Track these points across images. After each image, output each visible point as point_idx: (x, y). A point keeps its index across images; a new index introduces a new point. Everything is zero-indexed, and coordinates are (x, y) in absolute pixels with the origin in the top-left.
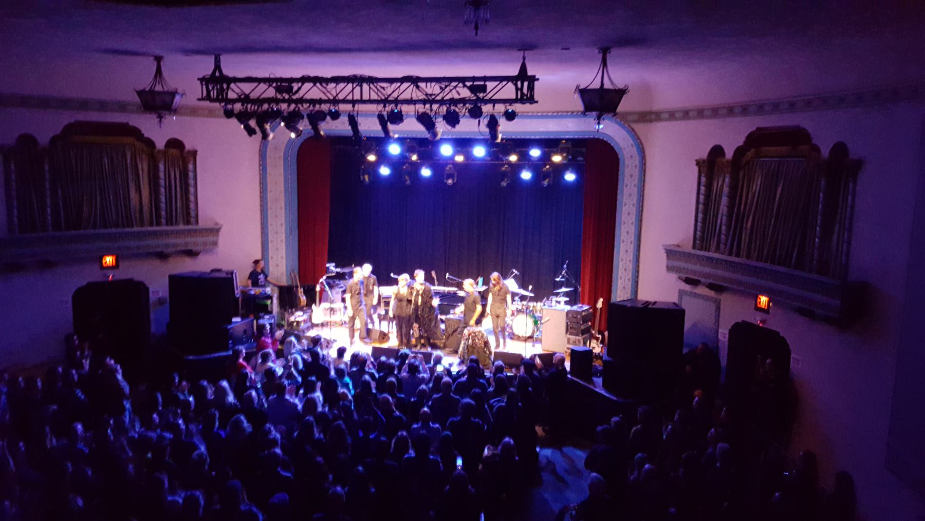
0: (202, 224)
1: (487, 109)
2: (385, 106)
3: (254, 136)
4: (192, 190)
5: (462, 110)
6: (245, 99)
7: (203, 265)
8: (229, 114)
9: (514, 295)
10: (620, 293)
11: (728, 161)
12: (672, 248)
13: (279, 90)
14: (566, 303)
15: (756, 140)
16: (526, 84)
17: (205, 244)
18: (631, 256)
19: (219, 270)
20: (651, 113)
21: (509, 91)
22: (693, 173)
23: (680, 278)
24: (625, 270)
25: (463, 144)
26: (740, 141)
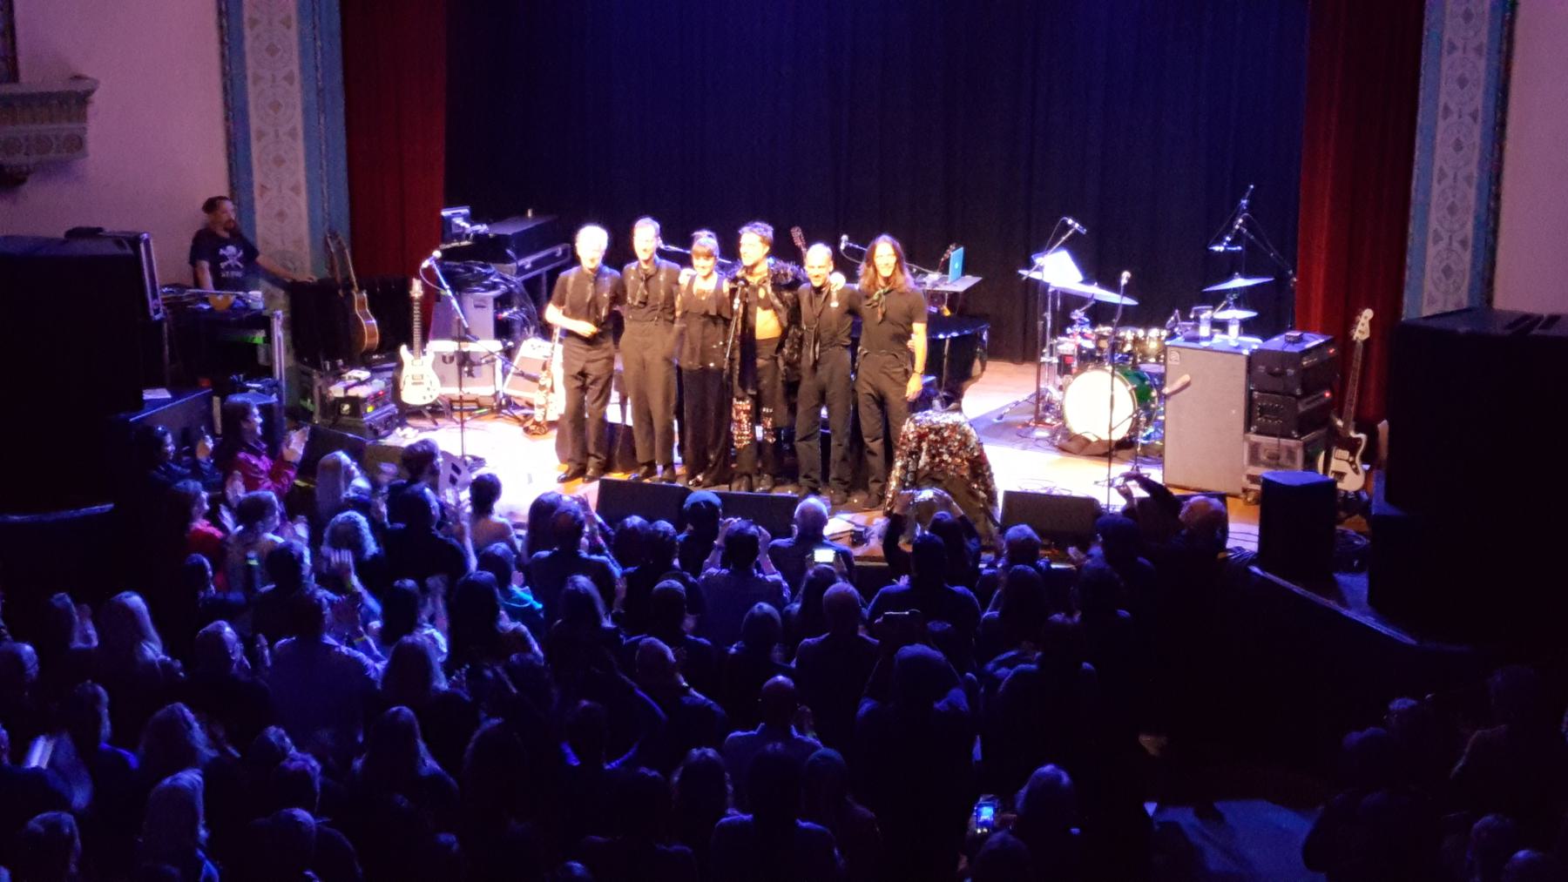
0: (31, 79)
9: (1071, 301)
19: (94, 233)
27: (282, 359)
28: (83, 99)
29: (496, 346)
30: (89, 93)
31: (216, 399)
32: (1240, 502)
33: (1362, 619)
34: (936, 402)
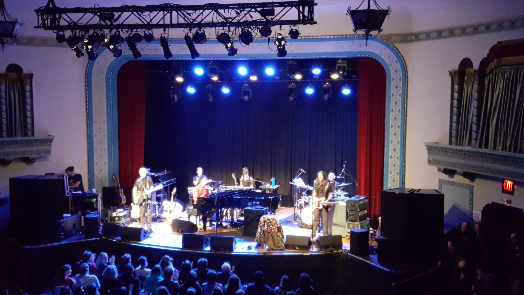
0: (37, 135)
1: (275, 29)
2: (190, 30)
3: (81, 57)
4: (28, 107)
5: (256, 33)
6: (73, 26)
7: (39, 169)
8: (60, 39)
9: (302, 190)
10: (391, 183)
11: (475, 71)
12: (432, 145)
13: (102, 17)
14: (345, 196)
15: (498, 51)
16: (306, 8)
17: (40, 152)
18: (399, 122)
19: (52, 174)
20: (411, 34)
21: (293, 14)
22: (445, 84)
23: (439, 170)
24: (394, 165)
25: (256, 65)
26: (485, 54)
27: (100, 207)
28: (51, 141)
29: (156, 203)
30: (52, 139)
31: (83, 217)
32: (345, 239)
33: (376, 265)
34: (269, 213)
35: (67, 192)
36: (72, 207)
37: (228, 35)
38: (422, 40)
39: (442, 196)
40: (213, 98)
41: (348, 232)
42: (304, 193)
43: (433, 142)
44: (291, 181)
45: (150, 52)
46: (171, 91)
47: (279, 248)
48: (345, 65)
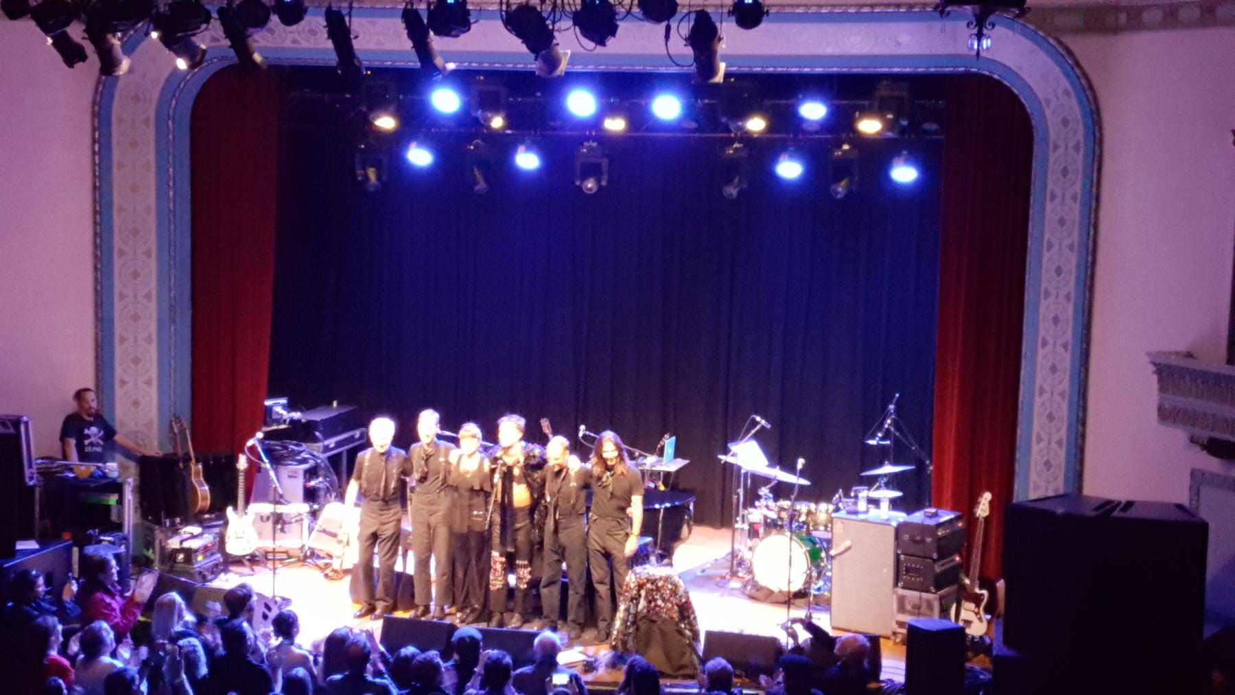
3: (79, 66)
9: (758, 480)
12: (1173, 360)
24: (1051, 417)
25: (624, 88)
29: (305, 508)
31: (75, 550)
32: (890, 643)
35: (27, 472)
36: (42, 517)
37: (540, 14)
38: (1150, 28)
39: (1203, 527)
40: (486, 180)
41: (901, 624)
42: (764, 491)
43: (1177, 353)
44: (726, 451)
45: (295, 41)
46: (358, 158)
47: (681, 672)
48: (904, 94)
